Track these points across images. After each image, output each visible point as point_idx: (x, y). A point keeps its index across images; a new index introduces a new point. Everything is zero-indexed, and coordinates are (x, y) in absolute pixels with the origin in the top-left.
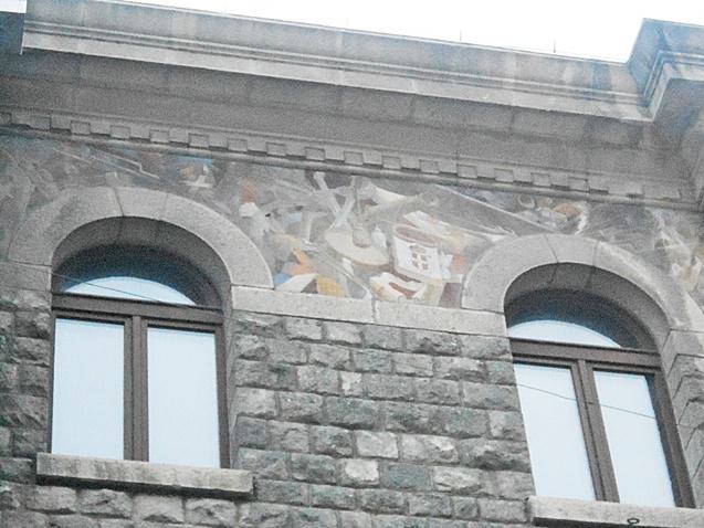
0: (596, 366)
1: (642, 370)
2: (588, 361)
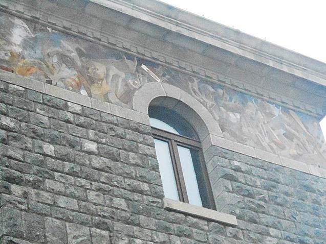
0: (178, 144)
1: (190, 147)
2: (175, 141)
